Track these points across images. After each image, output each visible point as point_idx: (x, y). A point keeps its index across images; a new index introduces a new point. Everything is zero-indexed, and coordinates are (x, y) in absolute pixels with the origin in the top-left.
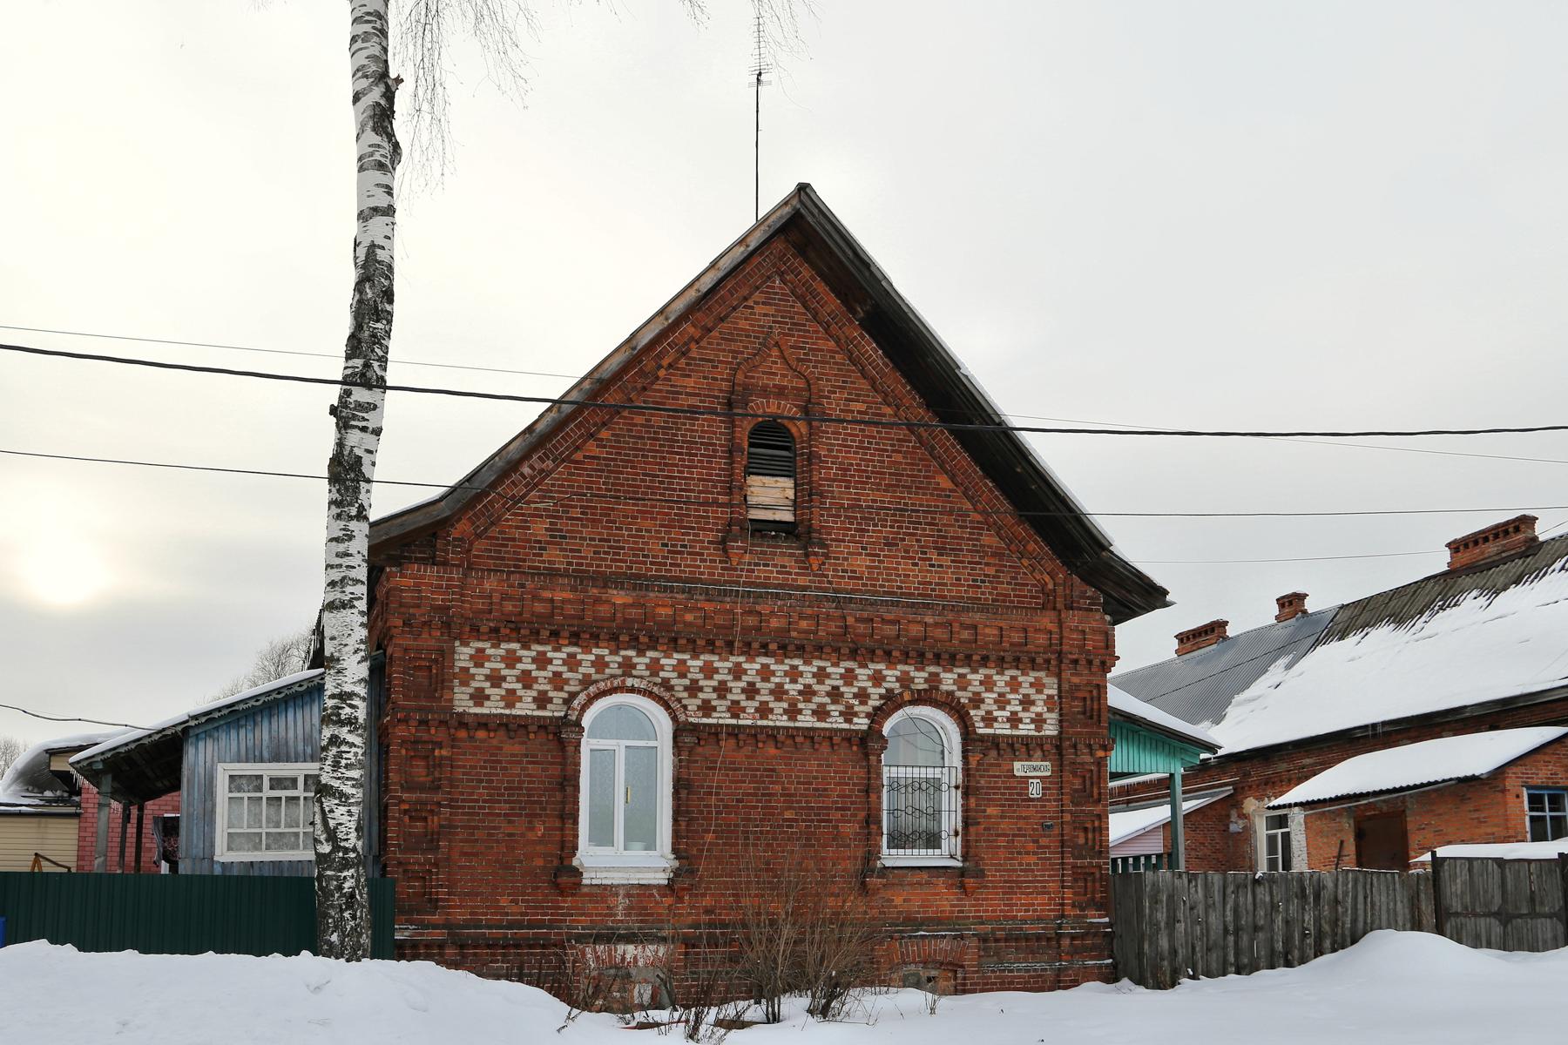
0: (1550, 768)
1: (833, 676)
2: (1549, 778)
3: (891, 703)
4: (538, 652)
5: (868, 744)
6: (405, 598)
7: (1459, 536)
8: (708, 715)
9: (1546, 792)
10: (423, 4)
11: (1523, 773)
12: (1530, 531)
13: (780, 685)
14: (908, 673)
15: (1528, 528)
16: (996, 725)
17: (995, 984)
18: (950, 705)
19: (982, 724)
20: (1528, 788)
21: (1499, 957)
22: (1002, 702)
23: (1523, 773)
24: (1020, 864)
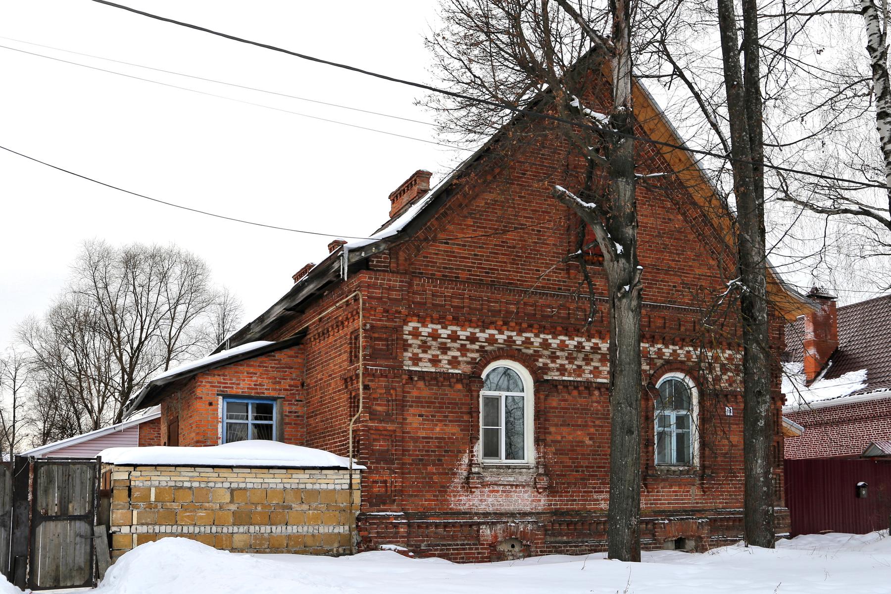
0: (254, 379)
1: (442, 336)
2: (253, 389)
3: (487, 357)
4: (433, 329)
5: (473, 380)
6: (492, 306)
7: (394, 190)
8: (416, 365)
9: (250, 402)
10: (532, 2)
11: (219, 383)
12: (424, 184)
13: (425, 342)
14: (437, 330)
15: (423, 181)
16: (420, 364)
17: (477, 558)
18: (528, 361)
19: (410, 363)
20: (225, 396)
21: (539, 563)
22: (425, 347)
23: (219, 383)
24: (583, 471)
